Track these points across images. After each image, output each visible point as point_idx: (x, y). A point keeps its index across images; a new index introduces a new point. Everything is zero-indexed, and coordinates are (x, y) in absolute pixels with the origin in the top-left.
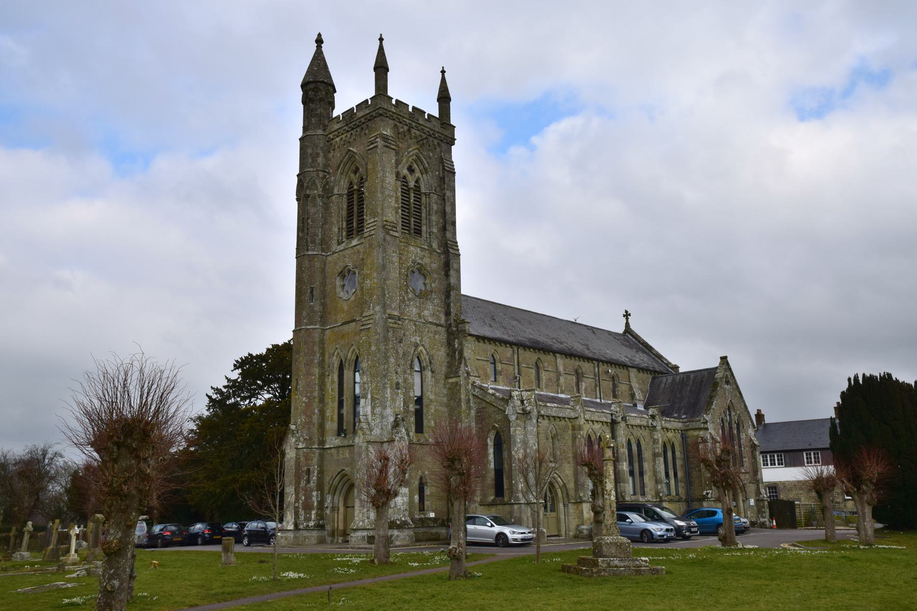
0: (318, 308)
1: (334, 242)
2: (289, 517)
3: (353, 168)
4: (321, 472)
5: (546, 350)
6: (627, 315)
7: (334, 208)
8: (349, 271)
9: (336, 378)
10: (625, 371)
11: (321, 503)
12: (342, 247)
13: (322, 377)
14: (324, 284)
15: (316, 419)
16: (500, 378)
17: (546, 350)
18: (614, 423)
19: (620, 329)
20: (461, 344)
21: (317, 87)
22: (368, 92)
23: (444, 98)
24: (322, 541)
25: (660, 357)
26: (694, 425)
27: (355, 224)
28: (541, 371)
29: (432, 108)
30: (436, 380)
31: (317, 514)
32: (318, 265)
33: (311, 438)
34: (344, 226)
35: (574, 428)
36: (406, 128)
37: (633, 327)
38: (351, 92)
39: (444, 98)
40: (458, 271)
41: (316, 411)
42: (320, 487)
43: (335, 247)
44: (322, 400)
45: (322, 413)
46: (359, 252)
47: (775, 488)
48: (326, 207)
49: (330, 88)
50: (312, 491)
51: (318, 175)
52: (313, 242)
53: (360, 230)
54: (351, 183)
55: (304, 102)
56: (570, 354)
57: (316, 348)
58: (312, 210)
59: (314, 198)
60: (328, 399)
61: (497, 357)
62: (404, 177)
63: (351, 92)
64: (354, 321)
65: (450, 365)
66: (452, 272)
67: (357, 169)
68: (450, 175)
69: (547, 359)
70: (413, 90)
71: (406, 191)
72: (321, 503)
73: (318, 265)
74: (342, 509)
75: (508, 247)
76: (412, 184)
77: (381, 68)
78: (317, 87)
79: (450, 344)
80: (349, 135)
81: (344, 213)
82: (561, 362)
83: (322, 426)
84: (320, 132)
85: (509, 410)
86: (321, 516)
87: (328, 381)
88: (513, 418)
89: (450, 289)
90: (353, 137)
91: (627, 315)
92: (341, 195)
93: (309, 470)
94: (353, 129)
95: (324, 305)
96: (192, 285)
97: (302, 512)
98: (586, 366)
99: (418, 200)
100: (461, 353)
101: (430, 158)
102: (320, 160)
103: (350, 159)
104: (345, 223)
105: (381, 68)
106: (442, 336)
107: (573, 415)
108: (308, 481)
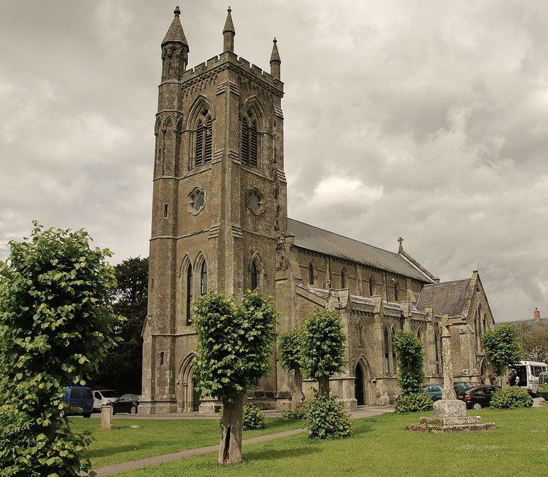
0: (171, 221)
1: (185, 168)
2: (146, 395)
3: (202, 110)
4: (173, 355)
8: (198, 192)
9: (186, 279)
10: (403, 281)
11: (173, 380)
13: (174, 277)
14: (176, 202)
15: (168, 312)
16: (315, 281)
21: (175, 49)
22: (218, 49)
23: (276, 62)
24: (174, 411)
27: (203, 154)
28: (346, 277)
29: (266, 68)
30: (268, 282)
31: (170, 389)
33: (165, 327)
34: (194, 156)
36: (247, 80)
38: (204, 49)
39: (276, 62)
40: (285, 196)
41: (169, 305)
42: (172, 368)
43: (185, 173)
44: (174, 297)
45: (174, 307)
46: (207, 176)
48: (179, 140)
49: (185, 48)
50: (165, 370)
51: (174, 115)
52: (168, 168)
54: (200, 122)
56: (366, 267)
57: (170, 255)
58: (168, 143)
60: (178, 296)
61: (314, 265)
62: (244, 119)
63: (204, 49)
64: (202, 232)
66: (280, 196)
67: (207, 112)
68: (275, 98)
69: (350, 268)
70: (254, 54)
71: (246, 128)
72: (173, 380)
75: (324, 190)
76: (250, 125)
77: (229, 33)
78: (175, 49)
80: (200, 84)
81: (194, 146)
83: (173, 318)
84: (176, 81)
86: (172, 391)
87: (179, 281)
90: (203, 86)
92: (191, 132)
93: (162, 353)
94: (204, 79)
95: (176, 219)
96: (25, 158)
97: (157, 388)
98: (377, 276)
99: (255, 139)
101: (264, 106)
103: (200, 102)
104: (194, 154)
105: (229, 33)
108: (162, 363)
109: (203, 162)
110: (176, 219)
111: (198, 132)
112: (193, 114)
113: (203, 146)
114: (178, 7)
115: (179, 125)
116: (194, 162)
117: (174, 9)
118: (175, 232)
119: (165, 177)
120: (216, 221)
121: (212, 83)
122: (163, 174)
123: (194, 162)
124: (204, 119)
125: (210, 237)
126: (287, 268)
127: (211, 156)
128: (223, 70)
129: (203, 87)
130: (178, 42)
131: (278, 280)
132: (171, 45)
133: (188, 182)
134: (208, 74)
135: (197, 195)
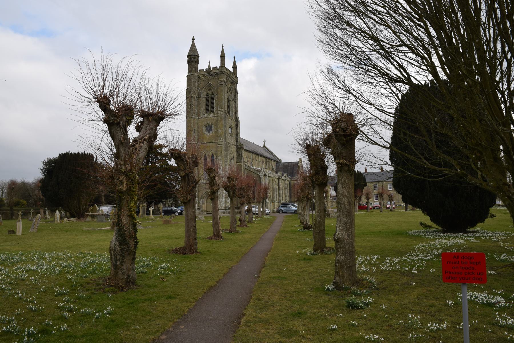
0: (196, 137)
5: (257, 154)
6: (264, 141)
7: (201, 102)
12: (204, 116)
17: (257, 154)
18: (279, 178)
19: (262, 146)
20: (241, 152)
21: (193, 58)
25: (275, 156)
26: (293, 179)
32: (196, 121)
35: (273, 180)
37: (266, 145)
43: (202, 116)
47: (391, 196)
53: (212, 111)
55: (189, 63)
59: (194, 98)
65: (237, 158)
73: (196, 121)
74: (205, 203)
78: (193, 58)
79: (237, 151)
81: (205, 104)
82: (260, 158)
84: (196, 74)
85: (260, 174)
88: (262, 177)
89: (237, 134)
91: (264, 141)
100: (242, 155)
102: (196, 84)
106: (235, 149)
107: (273, 176)
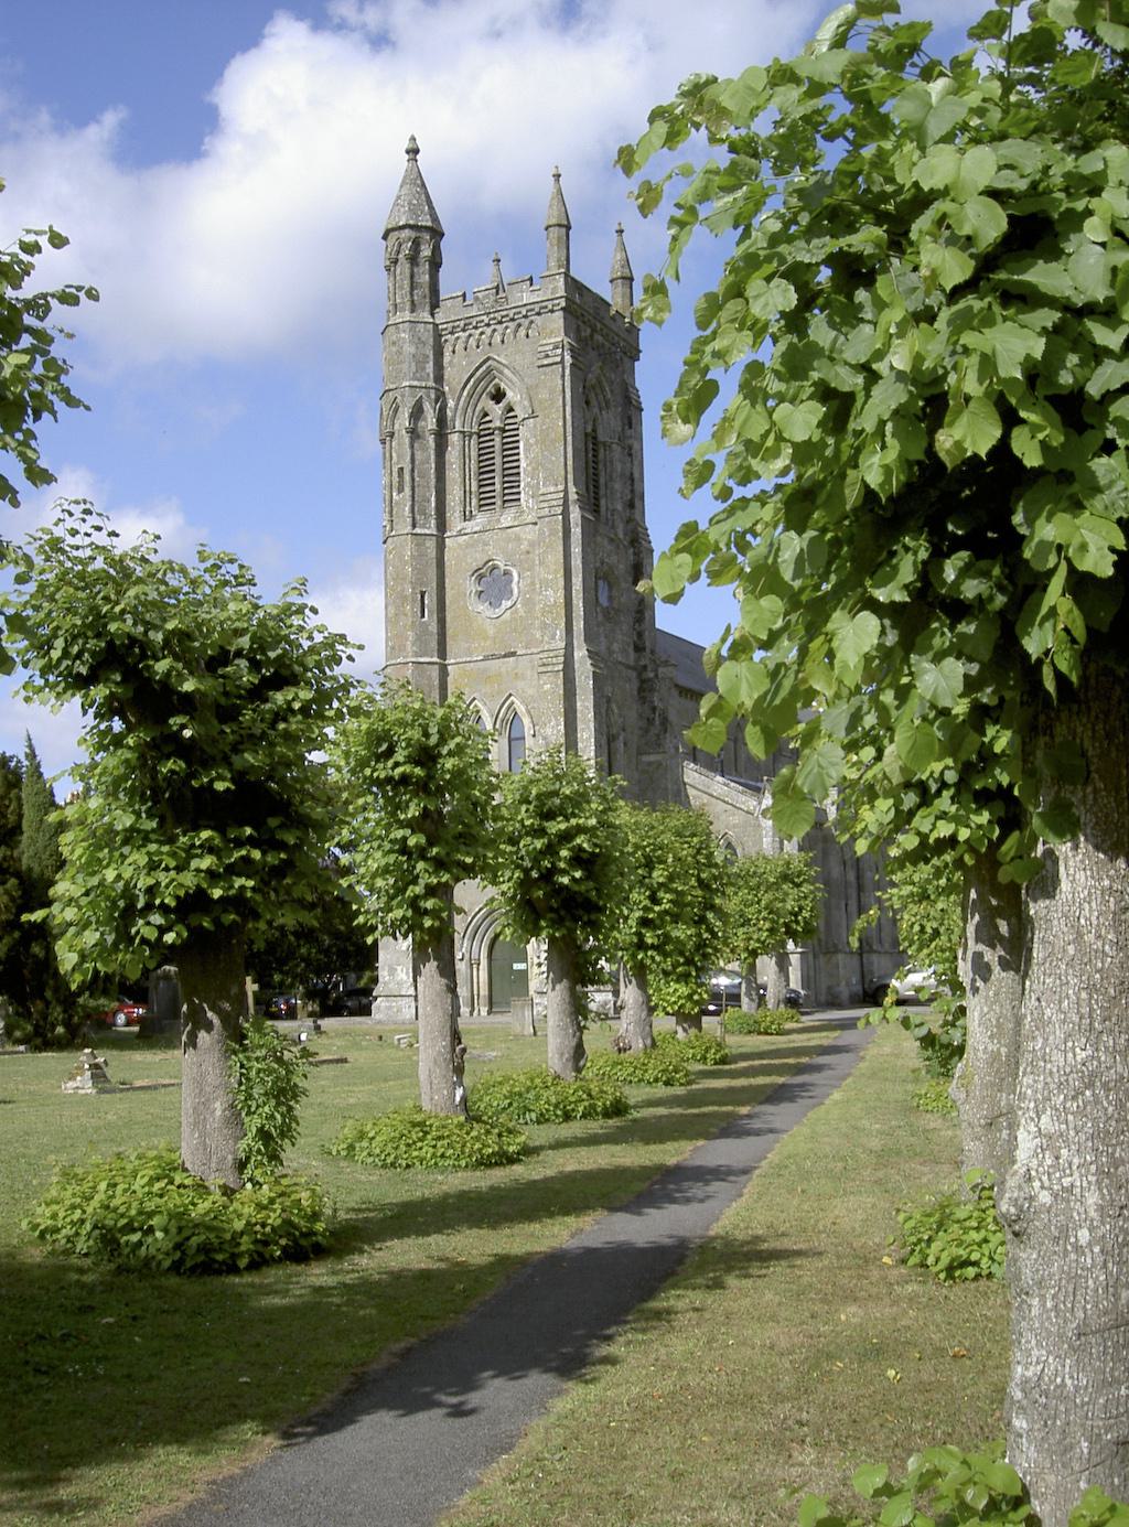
46: (518, 539)
51: (429, 396)
64: (513, 654)
80: (488, 331)
109: (499, 503)
110: (442, 622)
111: (480, 437)
112: (470, 396)
113: (498, 467)
114: (413, 139)
115: (442, 420)
116: (474, 501)
117: (406, 144)
118: (442, 653)
119: (418, 530)
120: (553, 637)
121: (522, 332)
122: (414, 526)
123: (474, 501)
124: (497, 410)
125: (544, 669)
126: (976, 1186)
127: (493, 471)
128: (552, 311)
129: (497, 337)
130: (426, 228)
131: (556, 363)
132: (406, 233)
133: (468, 546)
134: (511, 313)
135: (492, 582)
